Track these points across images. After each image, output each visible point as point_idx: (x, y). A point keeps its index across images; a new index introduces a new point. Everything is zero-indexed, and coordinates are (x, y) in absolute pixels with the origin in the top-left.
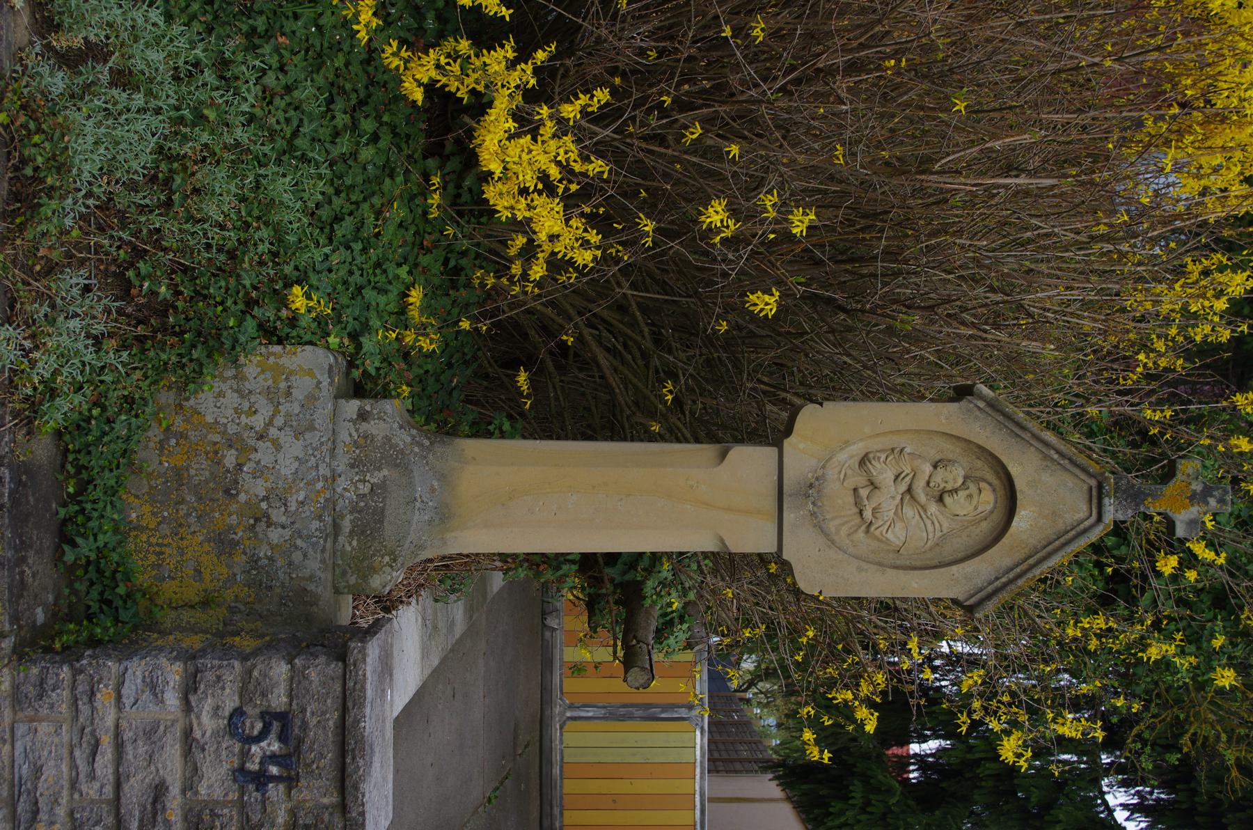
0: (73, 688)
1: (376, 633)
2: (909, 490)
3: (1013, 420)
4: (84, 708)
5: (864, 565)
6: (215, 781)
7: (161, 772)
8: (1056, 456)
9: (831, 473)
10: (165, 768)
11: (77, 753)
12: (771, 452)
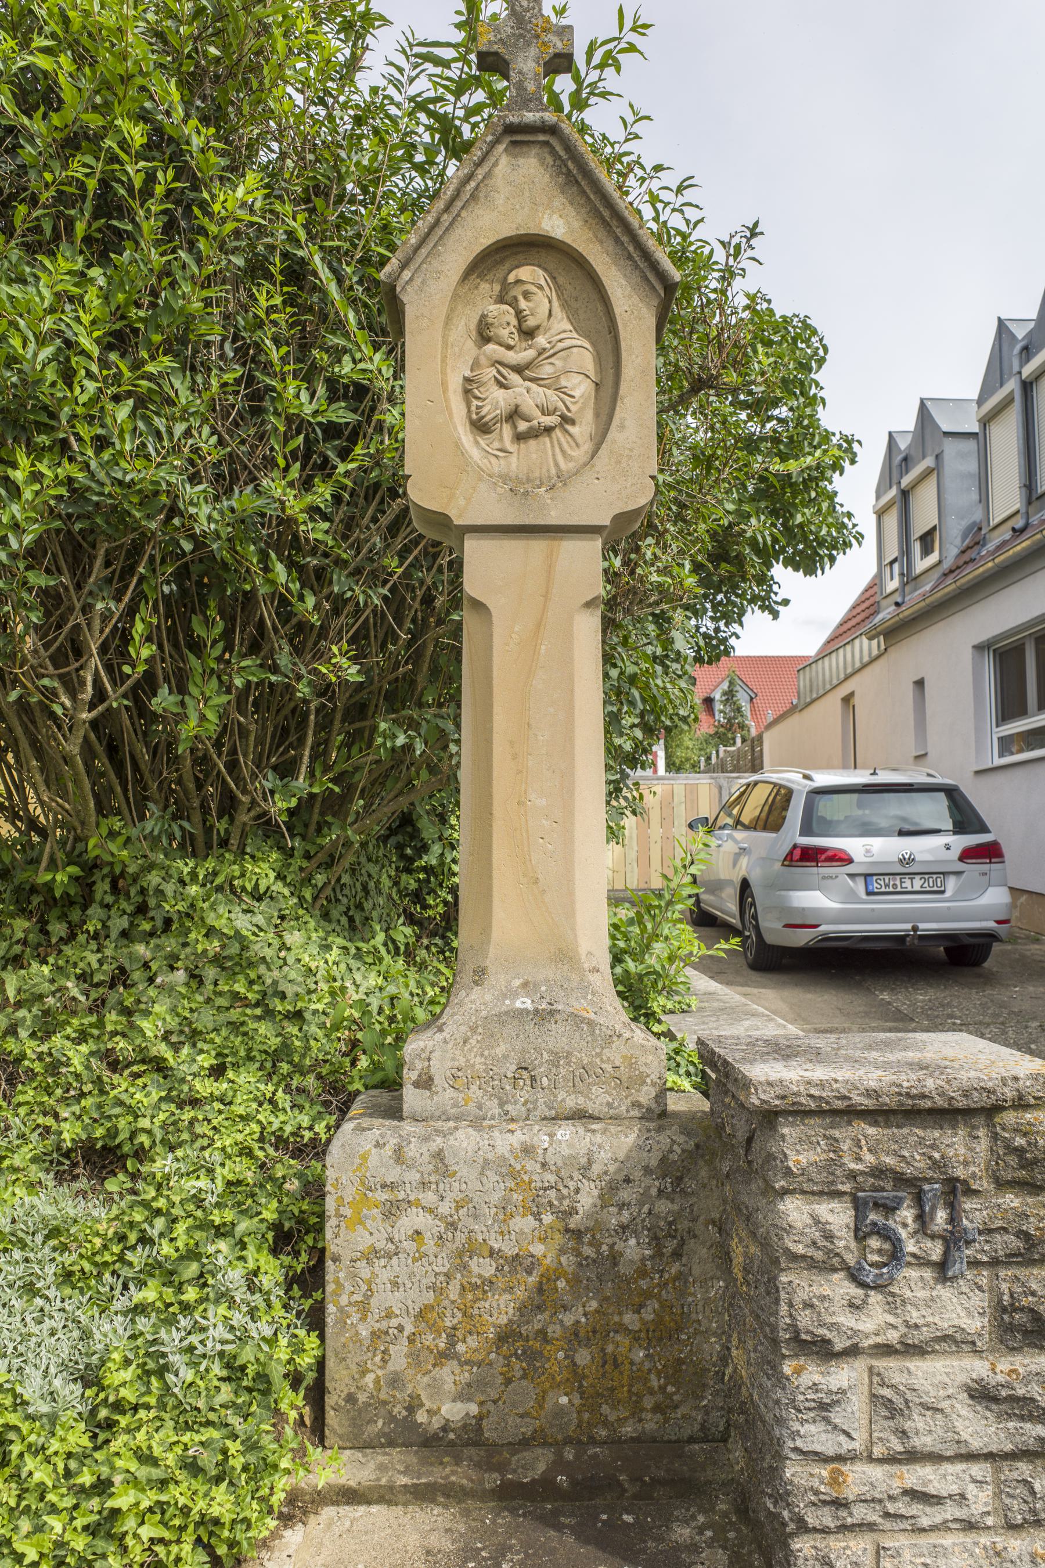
0: (825, 1531)
1: (725, 1062)
2: (519, 370)
3: (428, 235)
4: (860, 1513)
5: (616, 422)
6: (962, 1308)
7: (950, 1391)
8: (473, 184)
9: (497, 466)
10: (945, 1386)
11: (925, 1522)
12: (473, 549)
